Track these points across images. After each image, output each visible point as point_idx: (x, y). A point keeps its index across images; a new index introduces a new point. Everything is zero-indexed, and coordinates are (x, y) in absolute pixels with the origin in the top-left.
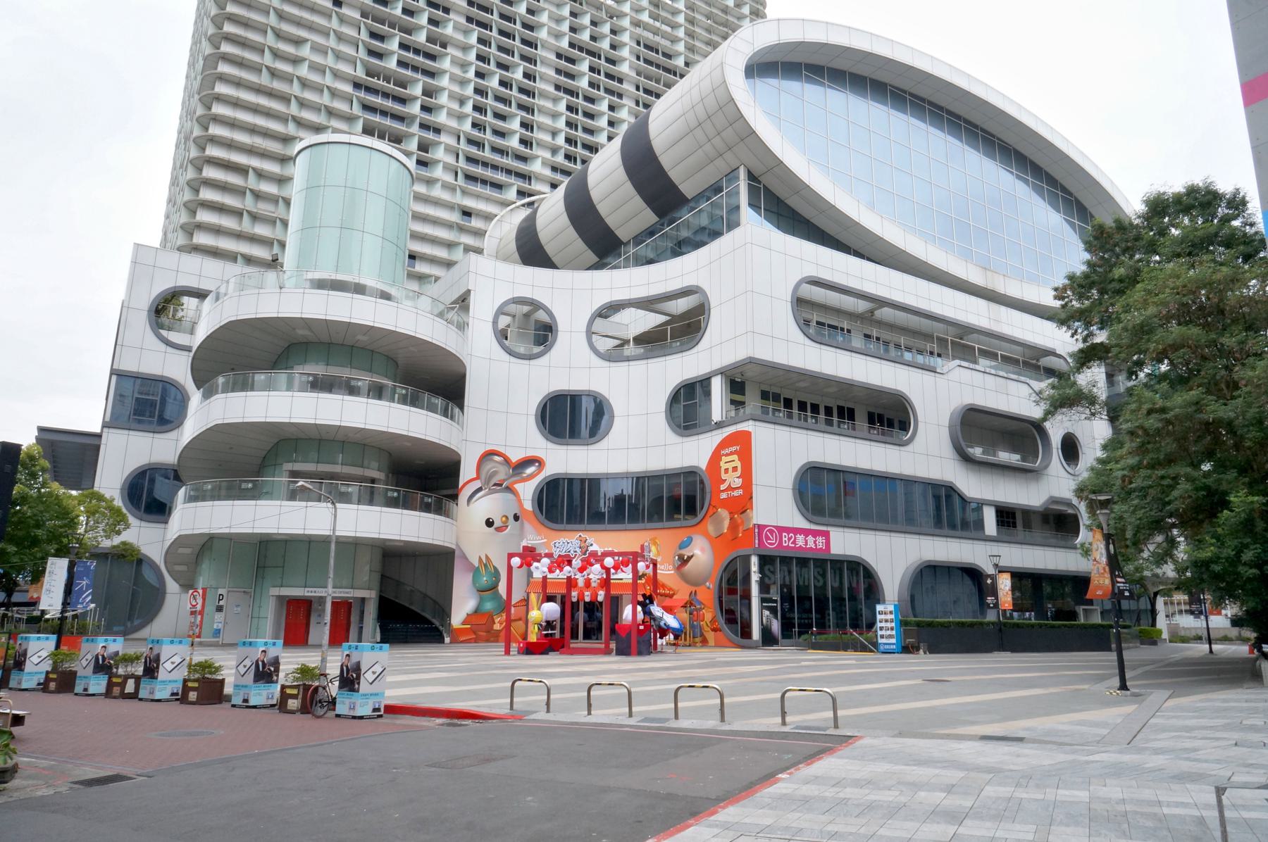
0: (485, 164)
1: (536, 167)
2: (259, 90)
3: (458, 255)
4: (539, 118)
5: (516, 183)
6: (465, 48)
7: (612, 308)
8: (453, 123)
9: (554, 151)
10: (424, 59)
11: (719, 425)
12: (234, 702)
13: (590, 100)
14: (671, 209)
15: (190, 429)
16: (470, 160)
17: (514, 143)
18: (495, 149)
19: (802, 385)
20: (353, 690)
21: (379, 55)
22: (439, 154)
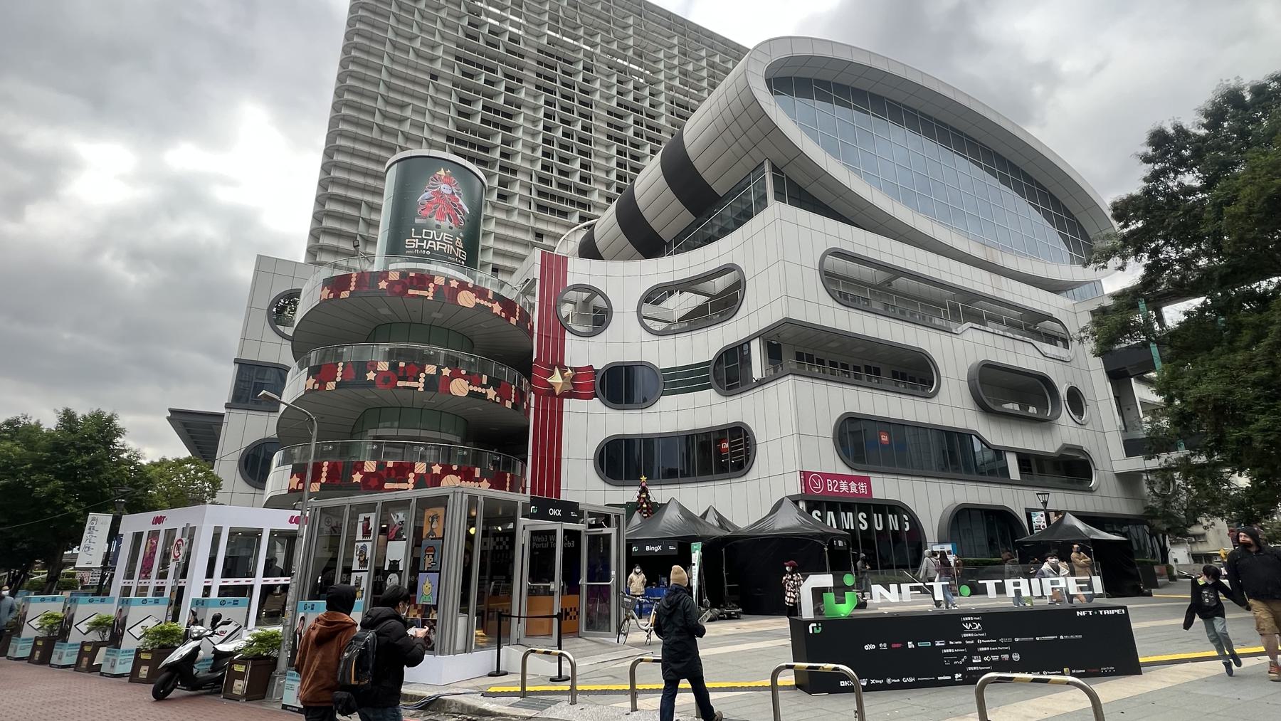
0: (553, 197)
2: (371, 143)
6: (536, 109)
8: (527, 165)
9: (609, 186)
10: (502, 118)
11: (761, 383)
14: (707, 204)
16: (541, 193)
18: (560, 185)
21: (467, 116)
22: (516, 188)
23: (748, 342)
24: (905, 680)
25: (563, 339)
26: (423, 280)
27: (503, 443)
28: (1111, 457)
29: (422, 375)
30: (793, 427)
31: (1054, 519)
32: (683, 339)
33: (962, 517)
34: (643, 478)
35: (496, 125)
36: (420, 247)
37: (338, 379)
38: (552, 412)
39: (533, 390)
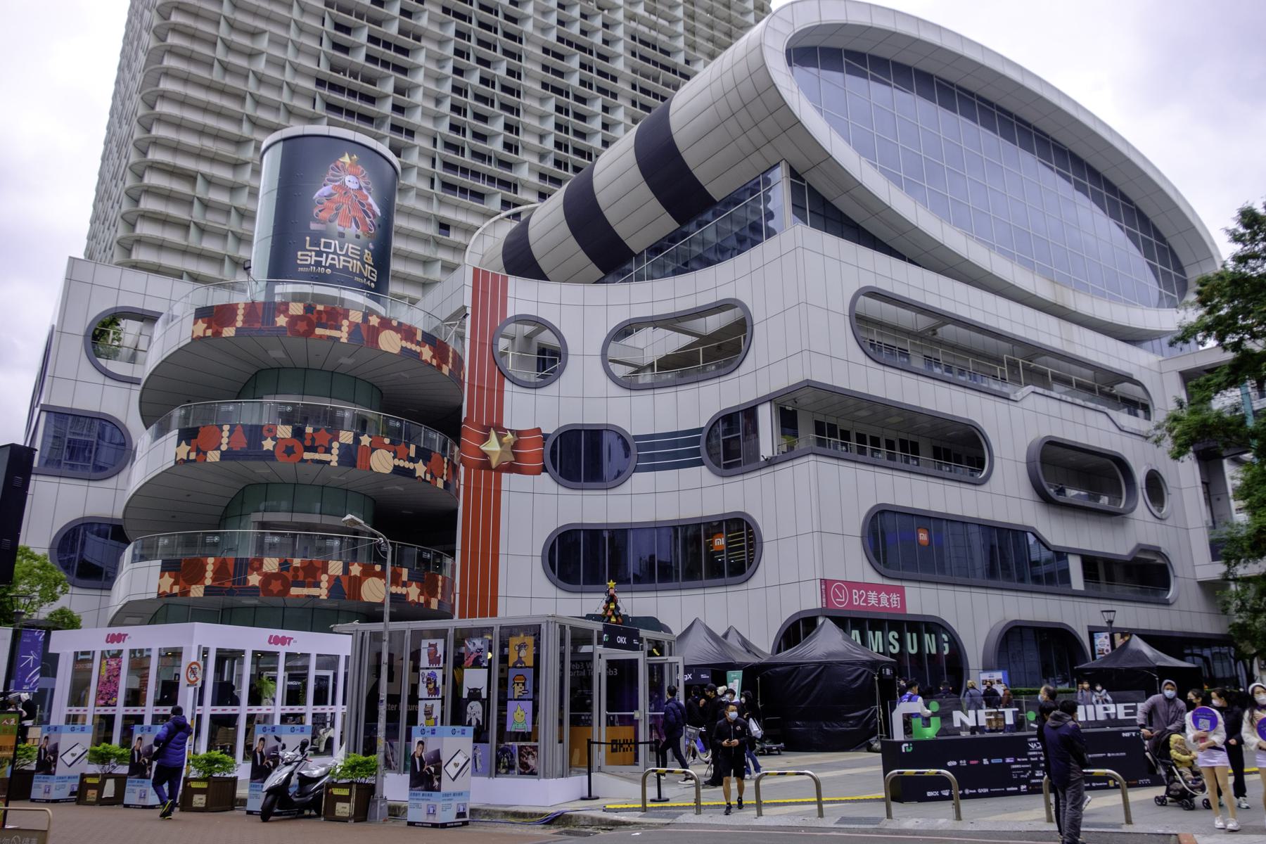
0: (465, 171)
1: (523, 174)
2: (209, 87)
3: (436, 273)
4: (524, 119)
5: (500, 193)
6: (442, 42)
7: (624, 331)
8: (429, 125)
9: (542, 156)
10: (395, 54)
11: (770, 462)
12: (249, 808)
13: (582, 100)
14: (695, 210)
15: (138, 474)
16: (448, 166)
17: (497, 146)
18: (475, 154)
19: (863, 413)
20: (431, 788)
21: (345, 49)
23: (750, 413)
24: (980, 791)
25: (501, 391)
26: (334, 314)
27: (420, 530)
28: (1195, 563)
29: (335, 445)
30: (812, 520)
31: (1119, 641)
32: (666, 398)
33: (1014, 638)
34: (611, 584)
35: (385, 64)
36: (318, 264)
37: (224, 447)
38: (487, 491)
39: (462, 460)
